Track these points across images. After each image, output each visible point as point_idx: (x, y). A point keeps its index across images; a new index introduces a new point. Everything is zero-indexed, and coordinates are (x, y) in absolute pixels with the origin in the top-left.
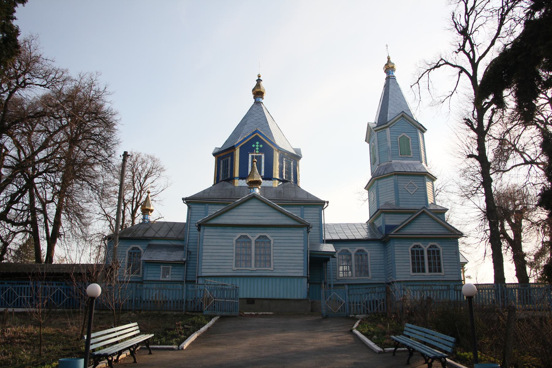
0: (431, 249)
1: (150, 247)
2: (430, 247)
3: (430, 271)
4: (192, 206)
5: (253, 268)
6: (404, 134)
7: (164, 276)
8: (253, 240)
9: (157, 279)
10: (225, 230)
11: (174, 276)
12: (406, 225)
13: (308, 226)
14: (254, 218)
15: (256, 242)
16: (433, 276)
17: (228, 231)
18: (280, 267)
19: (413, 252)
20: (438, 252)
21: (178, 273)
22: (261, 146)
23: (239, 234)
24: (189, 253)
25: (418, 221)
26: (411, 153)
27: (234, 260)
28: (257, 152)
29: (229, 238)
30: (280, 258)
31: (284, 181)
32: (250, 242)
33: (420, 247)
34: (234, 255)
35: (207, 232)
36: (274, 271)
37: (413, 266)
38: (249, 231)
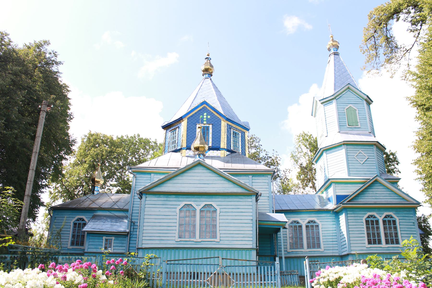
0: (78, 222)
1: (94, 217)
2: (385, 217)
3: (387, 242)
4: (137, 176)
5: (197, 240)
6: (351, 105)
7: (106, 248)
8: (198, 209)
9: (98, 251)
10: (168, 199)
11: (117, 248)
12: (359, 194)
13: (257, 194)
14: (199, 185)
15: (201, 211)
16: (391, 249)
17: (171, 199)
18: (227, 239)
19: (367, 222)
20: (394, 222)
21: (120, 245)
22: (209, 117)
23: (183, 202)
24: (132, 224)
25: (371, 190)
26: (359, 124)
27: (177, 231)
28: (205, 122)
29: (172, 206)
30: (227, 228)
31: (232, 152)
32: (195, 211)
33: (375, 217)
34: (177, 225)
35: (149, 200)
36: (220, 243)
37: (368, 237)
38: (193, 199)
